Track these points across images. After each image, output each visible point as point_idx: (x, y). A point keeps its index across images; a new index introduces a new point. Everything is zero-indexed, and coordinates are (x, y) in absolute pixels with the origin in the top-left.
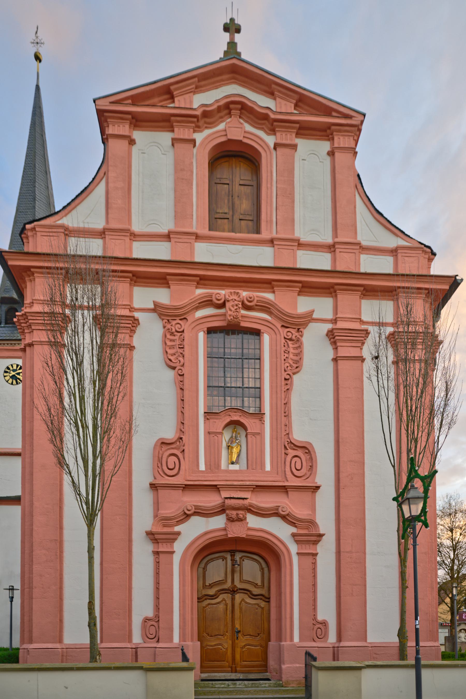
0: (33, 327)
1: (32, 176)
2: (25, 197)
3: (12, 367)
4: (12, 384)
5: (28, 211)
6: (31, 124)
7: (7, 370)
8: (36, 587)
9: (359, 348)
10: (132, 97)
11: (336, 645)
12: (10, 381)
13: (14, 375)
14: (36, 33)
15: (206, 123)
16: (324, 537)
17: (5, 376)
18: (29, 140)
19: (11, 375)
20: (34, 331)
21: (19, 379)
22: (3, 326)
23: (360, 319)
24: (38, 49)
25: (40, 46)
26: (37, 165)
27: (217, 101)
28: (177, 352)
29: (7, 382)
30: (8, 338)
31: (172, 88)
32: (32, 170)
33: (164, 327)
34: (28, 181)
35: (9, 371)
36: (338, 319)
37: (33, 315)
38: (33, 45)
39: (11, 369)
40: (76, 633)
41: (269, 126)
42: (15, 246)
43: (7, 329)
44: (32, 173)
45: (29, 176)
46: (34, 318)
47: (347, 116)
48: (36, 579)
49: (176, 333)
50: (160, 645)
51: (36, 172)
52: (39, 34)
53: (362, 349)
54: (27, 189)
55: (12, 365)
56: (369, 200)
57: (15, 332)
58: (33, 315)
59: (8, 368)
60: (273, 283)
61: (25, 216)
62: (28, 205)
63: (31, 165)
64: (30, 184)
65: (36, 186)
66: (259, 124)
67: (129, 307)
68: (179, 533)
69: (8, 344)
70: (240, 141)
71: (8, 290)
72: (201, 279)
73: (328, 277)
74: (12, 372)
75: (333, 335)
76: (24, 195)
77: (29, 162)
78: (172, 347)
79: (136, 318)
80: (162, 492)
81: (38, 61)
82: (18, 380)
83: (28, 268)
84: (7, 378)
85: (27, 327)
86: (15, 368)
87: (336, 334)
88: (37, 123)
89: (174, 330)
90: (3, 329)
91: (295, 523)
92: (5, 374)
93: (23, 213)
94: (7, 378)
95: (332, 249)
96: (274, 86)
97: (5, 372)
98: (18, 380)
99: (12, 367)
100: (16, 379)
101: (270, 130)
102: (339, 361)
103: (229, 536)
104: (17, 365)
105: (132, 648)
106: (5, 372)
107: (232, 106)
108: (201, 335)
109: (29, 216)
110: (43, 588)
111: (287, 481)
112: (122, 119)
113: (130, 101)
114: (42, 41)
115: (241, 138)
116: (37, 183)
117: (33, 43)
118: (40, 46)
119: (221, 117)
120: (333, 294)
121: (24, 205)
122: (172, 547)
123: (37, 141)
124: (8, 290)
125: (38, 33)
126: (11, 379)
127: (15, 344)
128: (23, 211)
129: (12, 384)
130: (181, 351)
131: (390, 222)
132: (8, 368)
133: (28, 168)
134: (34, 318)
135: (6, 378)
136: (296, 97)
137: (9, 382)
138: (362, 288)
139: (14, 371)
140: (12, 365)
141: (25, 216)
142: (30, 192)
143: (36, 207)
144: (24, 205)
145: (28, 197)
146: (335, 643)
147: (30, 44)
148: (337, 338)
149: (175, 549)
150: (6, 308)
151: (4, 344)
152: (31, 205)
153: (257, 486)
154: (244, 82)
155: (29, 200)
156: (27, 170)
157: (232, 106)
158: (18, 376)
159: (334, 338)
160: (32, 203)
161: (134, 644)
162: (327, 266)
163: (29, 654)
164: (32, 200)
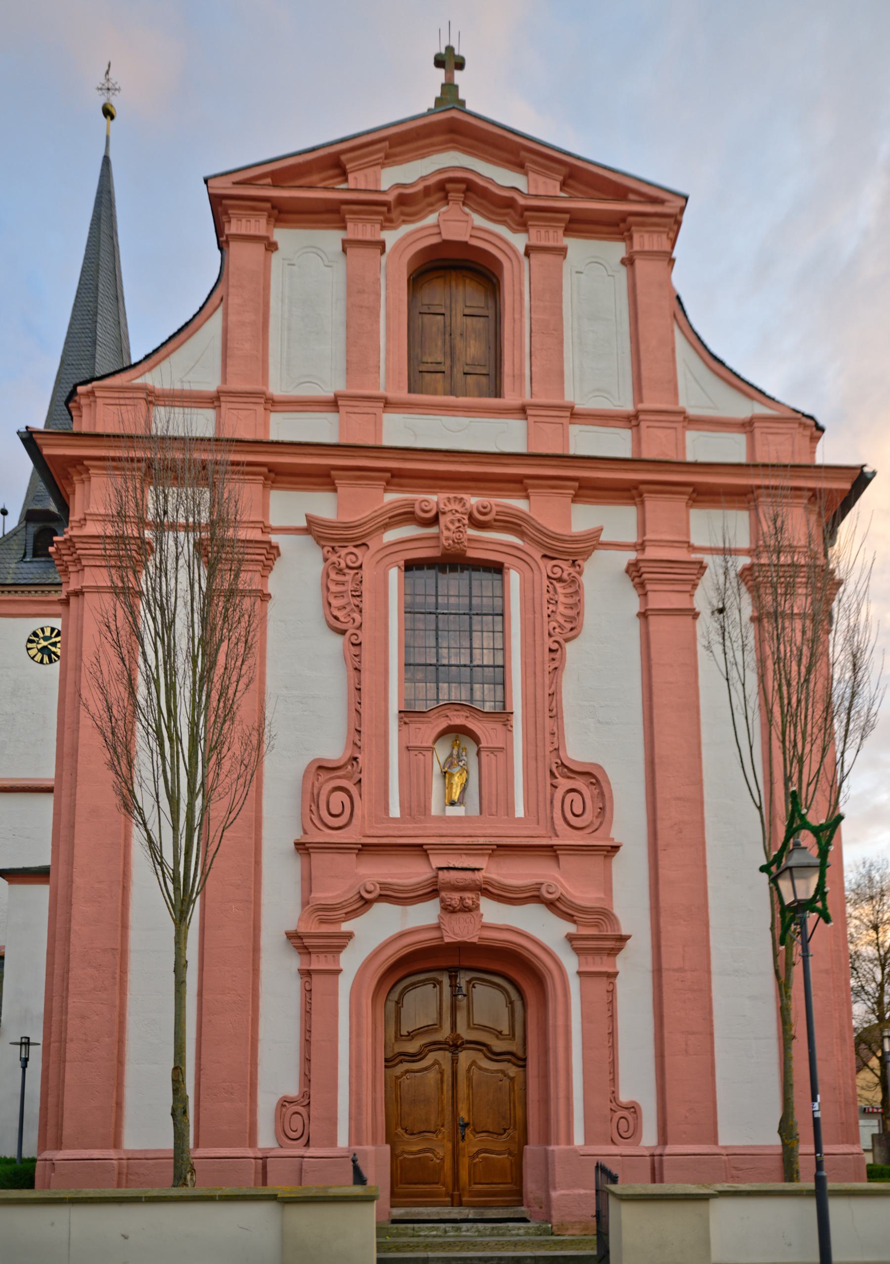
0: (84, 562)
1: (90, 304)
4: (41, 662)
5: (82, 362)
8: (72, 1040)
10: (272, 174)
11: (658, 1152)
12: (39, 657)
13: (45, 647)
14: (107, 73)
15: (403, 214)
16: (628, 941)
19: (39, 646)
20: (86, 569)
22: (28, 560)
23: (688, 542)
26: (100, 285)
27: (423, 178)
28: (349, 603)
29: (33, 658)
31: (343, 158)
33: (326, 560)
35: (36, 639)
36: (647, 543)
38: (100, 92)
39: (41, 635)
40: (147, 1129)
41: (517, 218)
44: (92, 299)
46: (87, 546)
47: (661, 202)
49: (347, 571)
50: (312, 1151)
53: (692, 596)
55: (42, 630)
56: (699, 338)
58: (85, 540)
59: (35, 634)
61: (75, 371)
64: (87, 317)
65: (99, 320)
66: (493, 213)
67: (261, 525)
68: (349, 936)
69: (36, 592)
70: (465, 244)
72: (393, 476)
74: (41, 641)
78: (339, 595)
80: (317, 859)
81: (109, 118)
84: (33, 652)
85: (74, 561)
86: (48, 633)
87: (643, 570)
89: (343, 565)
90: (29, 565)
91: (573, 916)
92: (30, 645)
94: (33, 652)
95: (634, 423)
96: (523, 154)
97: (30, 641)
100: (50, 653)
101: (519, 224)
102: (650, 618)
103: (447, 940)
104: (53, 630)
106: (30, 641)
107: (449, 186)
108: (394, 574)
111: (557, 836)
112: (254, 209)
113: (269, 181)
114: (117, 86)
115: (466, 238)
117: (101, 89)
119: (431, 205)
120: (637, 499)
122: (337, 961)
124: (41, 498)
125: (110, 73)
127: (49, 592)
130: (356, 601)
131: (738, 376)
132: (35, 634)
134: (87, 546)
136: (564, 170)
137: (36, 659)
138: (690, 489)
139: (46, 639)
140: (42, 630)
141: (75, 371)
145: (82, 340)
146: (655, 1147)
148: (645, 576)
149: (342, 965)
150: (36, 529)
151: (29, 592)
152: (87, 353)
153: (498, 846)
154: (471, 147)
157: (449, 186)
158: (53, 649)
159: (640, 576)
160: (89, 349)
161: (260, 1150)
162: (625, 451)
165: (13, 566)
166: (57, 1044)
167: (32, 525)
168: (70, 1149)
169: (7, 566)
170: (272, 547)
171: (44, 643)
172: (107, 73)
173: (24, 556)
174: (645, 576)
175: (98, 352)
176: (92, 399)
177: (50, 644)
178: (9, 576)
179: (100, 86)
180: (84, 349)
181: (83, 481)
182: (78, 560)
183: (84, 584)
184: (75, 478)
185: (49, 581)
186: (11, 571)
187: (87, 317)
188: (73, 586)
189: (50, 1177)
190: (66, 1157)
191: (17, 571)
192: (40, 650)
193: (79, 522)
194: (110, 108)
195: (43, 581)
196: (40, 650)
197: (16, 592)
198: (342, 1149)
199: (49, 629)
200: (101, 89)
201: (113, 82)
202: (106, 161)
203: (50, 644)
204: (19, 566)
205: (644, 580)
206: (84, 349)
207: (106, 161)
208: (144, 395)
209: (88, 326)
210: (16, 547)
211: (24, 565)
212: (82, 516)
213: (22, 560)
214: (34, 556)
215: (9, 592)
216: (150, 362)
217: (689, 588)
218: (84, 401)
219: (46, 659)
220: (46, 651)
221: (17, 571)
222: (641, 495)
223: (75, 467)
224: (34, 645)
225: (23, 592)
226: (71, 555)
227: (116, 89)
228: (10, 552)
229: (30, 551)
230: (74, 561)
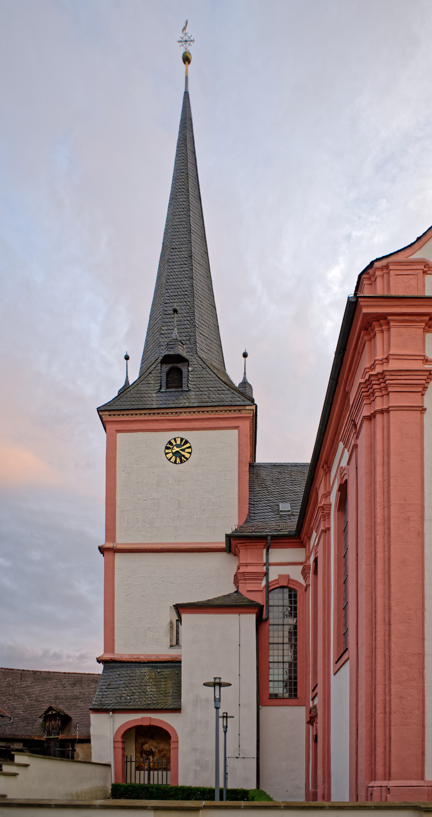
0: (390, 389)
1: (184, 203)
2: (178, 230)
3: (176, 442)
4: (175, 462)
5: (182, 246)
6: (179, 140)
7: (169, 446)
9: (420, 393)
12: (173, 459)
13: (178, 452)
14: (184, 29)
17: (166, 454)
18: (176, 160)
19: (174, 451)
20: (390, 394)
21: (184, 456)
22: (163, 391)
23: (425, 356)
24: (186, 49)
25: (189, 45)
26: (190, 189)
29: (169, 460)
30: (173, 406)
32: (185, 196)
34: (180, 210)
35: (171, 446)
36: (390, 357)
37: (393, 373)
38: (180, 44)
39: (174, 444)
42: (169, 291)
43: (169, 394)
44: (185, 200)
45: (181, 203)
46: (393, 378)
48: (395, 702)
50: (392, 783)
51: (190, 198)
52: (187, 30)
53: (423, 395)
54: (179, 220)
55: (175, 439)
57: (181, 397)
58: (393, 373)
59: (170, 443)
60: (389, 318)
61: (178, 253)
62: (182, 240)
63: (183, 190)
64: (182, 213)
65: (191, 215)
67: (422, 358)
69: (172, 413)
71: (173, 346)
73: (407, 306)
74: (175, 448)
75: (383, 378)
76: (176, 227)
77: (181, 187)
79: (382, 372)
81: (187, 63)
82: (183, 458)
83: (384, 316)
84: (169, 456)
85: (380, 389)
86: (179, 442)
87: (387, 378)
88: (188, 138)
90: (165, 394)
92: (167, 451)
93: (175, 250)
94: (169, 456)
97: (167, 448)
98: (183, 458)
99: (176, 442)
100: (181, 456)
104: (182, 440)
105: (427, 786)
106: (167, 448)
109: (184, 253)
110: (403, 713)
114: (192, 39)
116: (191, 212)
117: (181, 42)
118: (189, 45)
121: (177, 240)
123: (189, 160)
124: (173, 346)
125: (187, 28)
126: (174, 457)
127: (181, 413)
128: (176, 247)
129: (175, 462)
132: (170, 443)
133: (179, 194)
134: (393, 378)
135: (168, 456)
137: (171, 460)
138: (427, 318)
139: (178, 446)
140: (175, 439)
141: (178, 253)
142: (184, 223)
143: (192, 241)
144: (177, 240)
145: (181, 230)
147: (178, 43)
148: (388, 382)
150: (168, 368)
151: (167, 413)
152: (185, 239)
155: (183, 233)
156: (179, 197)
158: (183, 453)
159: (385, 382)
160: (186, 236)
163: (389, 793)
164: (186, 233)
165: (154, 395)
166: (382, 715)
167: (165, 366)
168: (396, 780)
169: (150, 395)
170: (382, 374)
171: (176, 449)
172: (184, 29)
173: (160, 388)
174: (388, 382)
175: (192, 238)
176: (385, 271)
177: (181, 450)
178: (153, 403)
179: (180, 39)
180: (182, 236)
181: (382, 331)
182: (386, 388)
183: (390, 405)
184: (376, 329)
185: (181, 405)
186: (154, 399)
187: (182, 213)
188: (379, 405)
189: (386, 797)
190: (396, 785)
191: (158, 399)
192: (174, 454)
193: (382, 360)
194: (188, 56)
195: (177, 405)
196: (174, 454)
197: (158, 414)
198: (427, 781)
199: (179, 439)
200: (181, 42)
201: (189, 35)
202: (186, 95)
203: (181, 450)
204: (158, 395)
205: (387, 384)
206: (182, 236)
207: (186, 95)
208: (422, 267)
209: (184, 219)
210: (153, 382)
211: (161, 394)
212: (385, 356)
213: (159, 391)
214: (167, 388)
215: (154, 414)
216: (421, 242)
217: (420, 389)
218: (378, 273)
219: (178, 461)
220: (178, 454)
221: (158, 399)
222: (388, 323)
223: (379, 321)
224: (170, 451)
225: (163, 413)
226: (380, 384)
227: (192, 41)
228: (149, 385)
229: (164, 384)
230: (380, 389)
